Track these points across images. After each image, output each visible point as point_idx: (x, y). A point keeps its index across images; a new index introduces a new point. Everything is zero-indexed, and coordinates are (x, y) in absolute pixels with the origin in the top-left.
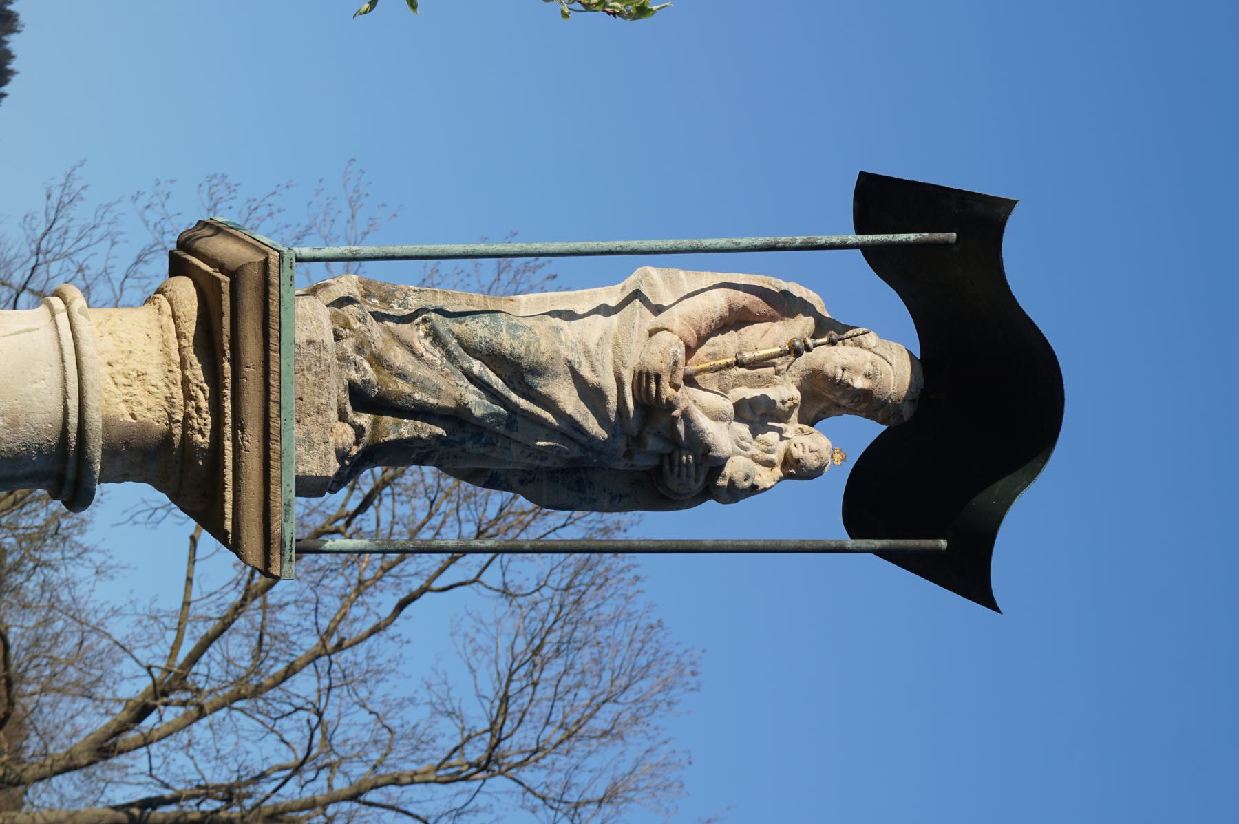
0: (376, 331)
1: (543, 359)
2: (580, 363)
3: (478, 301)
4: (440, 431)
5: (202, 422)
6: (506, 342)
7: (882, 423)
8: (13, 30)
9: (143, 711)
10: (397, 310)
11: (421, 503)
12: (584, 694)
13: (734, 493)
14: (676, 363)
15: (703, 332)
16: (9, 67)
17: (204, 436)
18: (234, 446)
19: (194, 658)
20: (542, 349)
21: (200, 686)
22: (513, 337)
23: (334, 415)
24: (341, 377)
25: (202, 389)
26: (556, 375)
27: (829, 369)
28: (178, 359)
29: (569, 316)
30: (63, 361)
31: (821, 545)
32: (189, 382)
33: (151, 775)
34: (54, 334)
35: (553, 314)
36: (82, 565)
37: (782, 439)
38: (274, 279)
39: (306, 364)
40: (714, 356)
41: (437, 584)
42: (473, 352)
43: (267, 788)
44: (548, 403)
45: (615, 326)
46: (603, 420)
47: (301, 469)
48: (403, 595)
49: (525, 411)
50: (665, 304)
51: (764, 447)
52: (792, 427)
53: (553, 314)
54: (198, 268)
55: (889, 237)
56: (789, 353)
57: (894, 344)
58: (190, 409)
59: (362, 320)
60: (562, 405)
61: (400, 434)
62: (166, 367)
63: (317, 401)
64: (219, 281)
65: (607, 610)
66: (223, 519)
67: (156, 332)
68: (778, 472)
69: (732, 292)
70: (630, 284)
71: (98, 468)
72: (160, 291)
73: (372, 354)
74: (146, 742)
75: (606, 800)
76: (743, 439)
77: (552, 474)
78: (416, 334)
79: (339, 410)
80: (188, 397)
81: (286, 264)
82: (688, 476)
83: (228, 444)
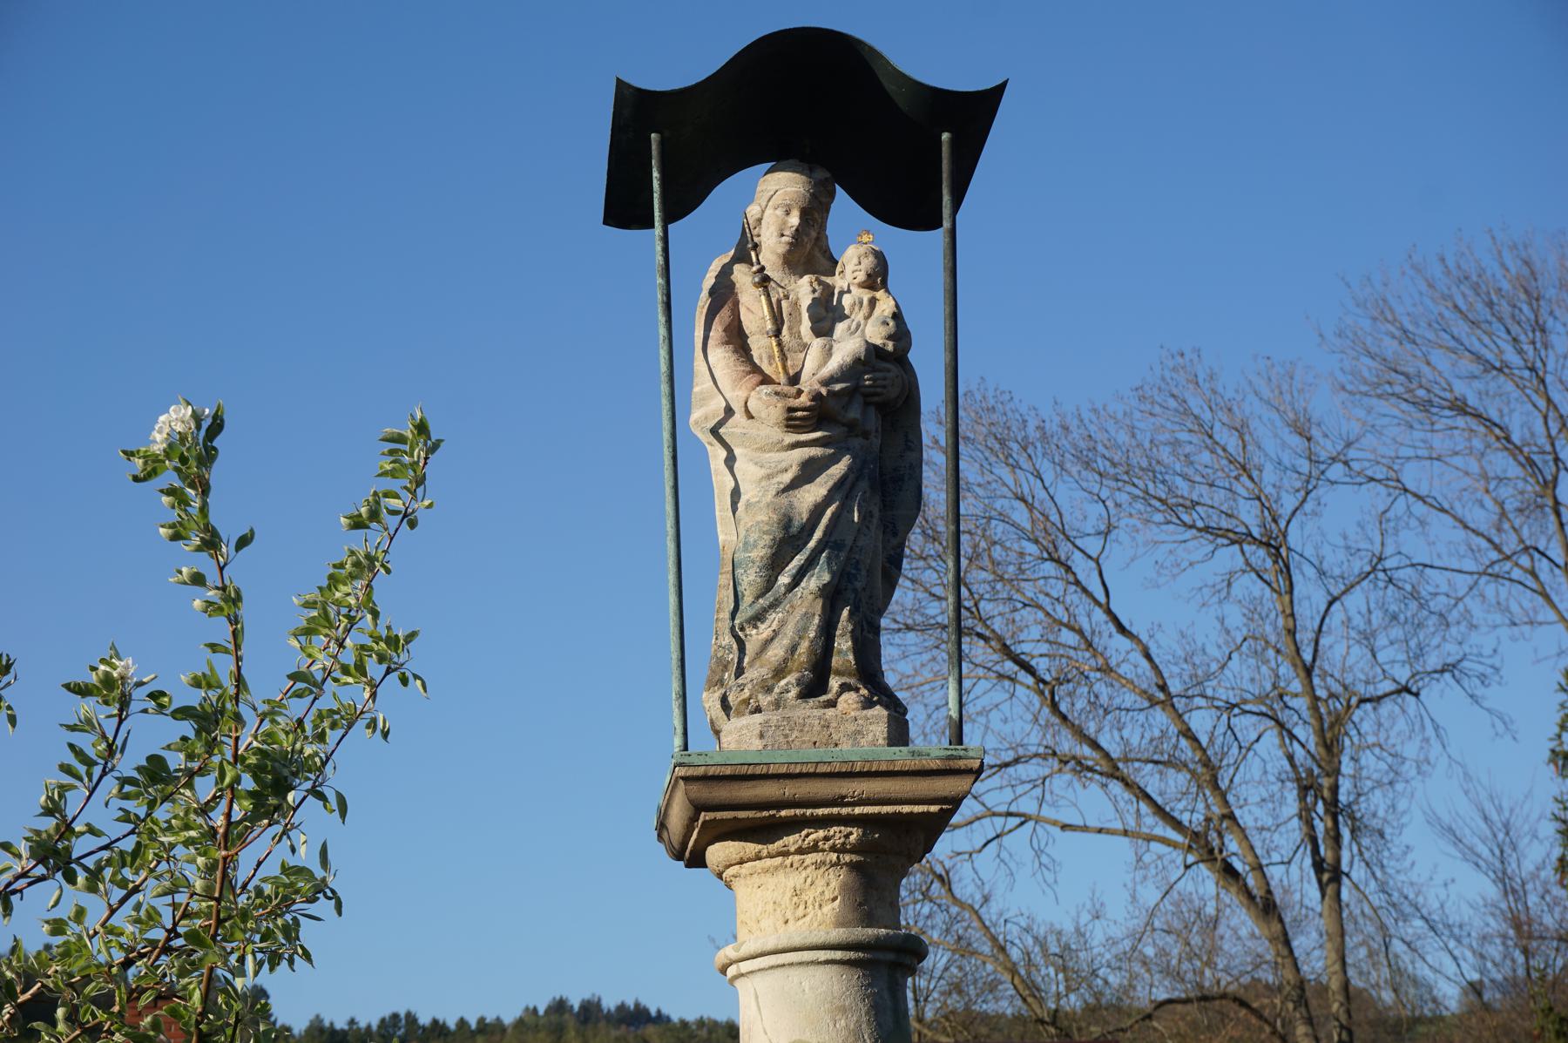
0: (753, 674)
1: (775, 517)
2: (779, 483)
3: (725, 580)
4: (845, 613)
5: (838, 835)
6: (760, 553)
7: (832, 195)
8: (598, 1004)
9: (1229, 872)
10: (733, 657)
11: (1027, 614)
12: (1206, 457)
13: (901, 332)
14: (777, 393)
15: (748, 369)
16: (632, 1007)
17: (851, 833)
18: (860, 805)
19: (1177, 825)
20: (766, 519)
21: (1202, 818)
22: (755, 546)
23: (830, 712)
24: (794, 707)
25: (807, 836)
26: (791, 505)
27: (782, 249)
28: (780, 859)
29: (736, 494)
30: (784, 965)
31: (948, 252)
32: (800, 847)
33: (1289, 863)
34: (759, 974)
35: (734, 510)
36: (1092, 932)
37: (849, 291)
38: (700, 771)
39: (782, 739)
40: (771, 358)
41: (1102, 599)
42: (770, 583)
43: (1299, 753)
44: (817, 511)
45: (745, 451)
46: (833, 460)
47: (881, 741)
48: (1112, 628)
49: (824, 533)
50: (724, 404)
51: (857, 308)
52: (838, 282)
53: (734, 510)
54: (696, 841)
55: (656, 196)
56: (766, 287)
57: (759, 189)
58: (826, 846)
59: (742, 688)
60: (819, 499)
61: (848, 649)
62: (788, 870)
63: (817, 728)
64: (705, 822)
65: (1123, 437)
66: (928, 813)
67: (756, 879)
68: (880, 294)
69: (711, 343)
70: (706, 438)
71: (883, 931)
72: (720, 876)
73: (773, 677)
74: (1259, 868)
75: (1209, 441)
76: (849, 328)
77: (886, 506)
78: (755, 637)
79: (825, 707)
80: (814, 848)
81: (686, 760)
82: (885, 379)
83: (858, 810)
